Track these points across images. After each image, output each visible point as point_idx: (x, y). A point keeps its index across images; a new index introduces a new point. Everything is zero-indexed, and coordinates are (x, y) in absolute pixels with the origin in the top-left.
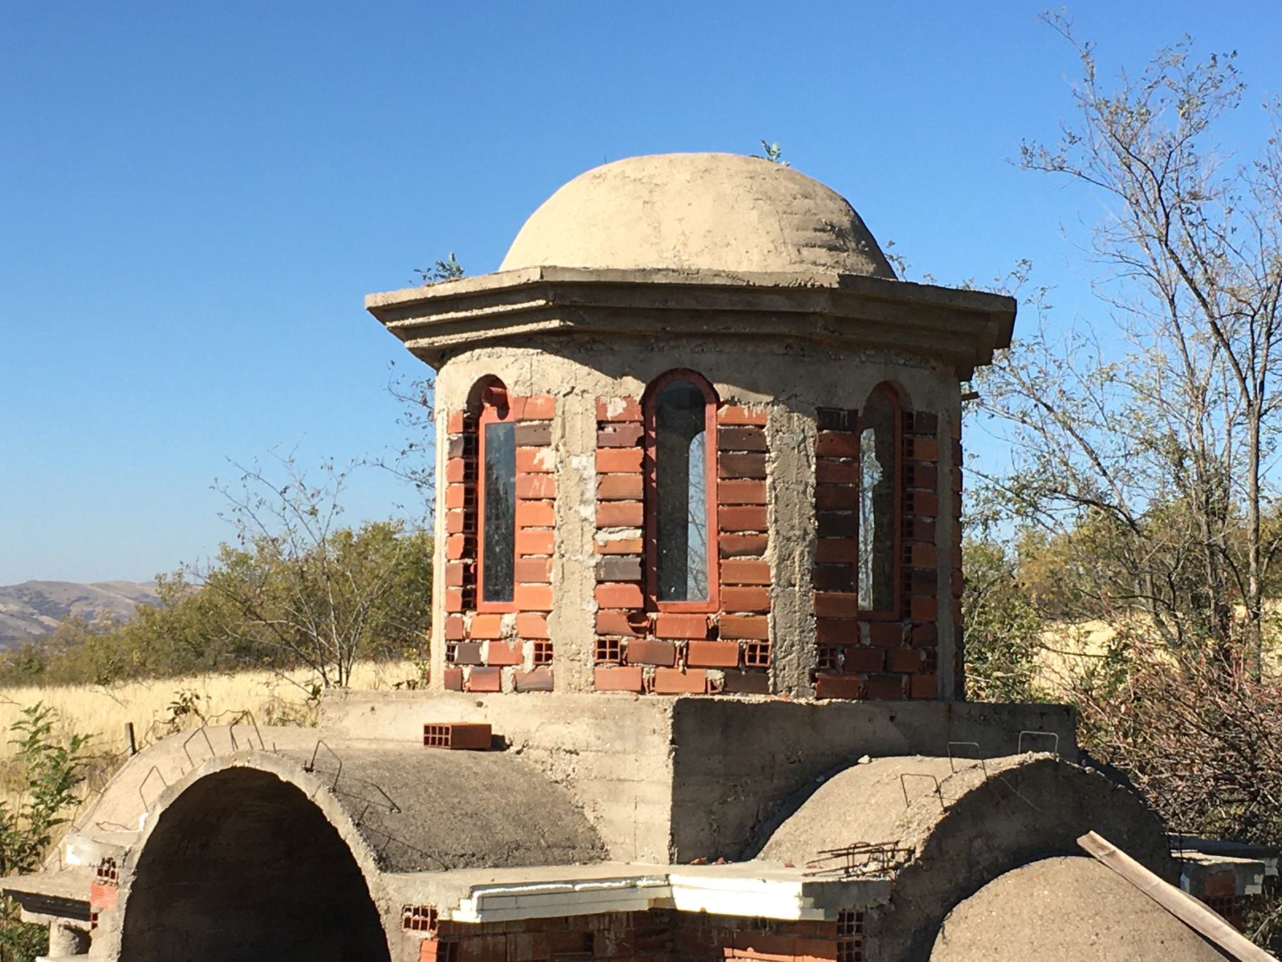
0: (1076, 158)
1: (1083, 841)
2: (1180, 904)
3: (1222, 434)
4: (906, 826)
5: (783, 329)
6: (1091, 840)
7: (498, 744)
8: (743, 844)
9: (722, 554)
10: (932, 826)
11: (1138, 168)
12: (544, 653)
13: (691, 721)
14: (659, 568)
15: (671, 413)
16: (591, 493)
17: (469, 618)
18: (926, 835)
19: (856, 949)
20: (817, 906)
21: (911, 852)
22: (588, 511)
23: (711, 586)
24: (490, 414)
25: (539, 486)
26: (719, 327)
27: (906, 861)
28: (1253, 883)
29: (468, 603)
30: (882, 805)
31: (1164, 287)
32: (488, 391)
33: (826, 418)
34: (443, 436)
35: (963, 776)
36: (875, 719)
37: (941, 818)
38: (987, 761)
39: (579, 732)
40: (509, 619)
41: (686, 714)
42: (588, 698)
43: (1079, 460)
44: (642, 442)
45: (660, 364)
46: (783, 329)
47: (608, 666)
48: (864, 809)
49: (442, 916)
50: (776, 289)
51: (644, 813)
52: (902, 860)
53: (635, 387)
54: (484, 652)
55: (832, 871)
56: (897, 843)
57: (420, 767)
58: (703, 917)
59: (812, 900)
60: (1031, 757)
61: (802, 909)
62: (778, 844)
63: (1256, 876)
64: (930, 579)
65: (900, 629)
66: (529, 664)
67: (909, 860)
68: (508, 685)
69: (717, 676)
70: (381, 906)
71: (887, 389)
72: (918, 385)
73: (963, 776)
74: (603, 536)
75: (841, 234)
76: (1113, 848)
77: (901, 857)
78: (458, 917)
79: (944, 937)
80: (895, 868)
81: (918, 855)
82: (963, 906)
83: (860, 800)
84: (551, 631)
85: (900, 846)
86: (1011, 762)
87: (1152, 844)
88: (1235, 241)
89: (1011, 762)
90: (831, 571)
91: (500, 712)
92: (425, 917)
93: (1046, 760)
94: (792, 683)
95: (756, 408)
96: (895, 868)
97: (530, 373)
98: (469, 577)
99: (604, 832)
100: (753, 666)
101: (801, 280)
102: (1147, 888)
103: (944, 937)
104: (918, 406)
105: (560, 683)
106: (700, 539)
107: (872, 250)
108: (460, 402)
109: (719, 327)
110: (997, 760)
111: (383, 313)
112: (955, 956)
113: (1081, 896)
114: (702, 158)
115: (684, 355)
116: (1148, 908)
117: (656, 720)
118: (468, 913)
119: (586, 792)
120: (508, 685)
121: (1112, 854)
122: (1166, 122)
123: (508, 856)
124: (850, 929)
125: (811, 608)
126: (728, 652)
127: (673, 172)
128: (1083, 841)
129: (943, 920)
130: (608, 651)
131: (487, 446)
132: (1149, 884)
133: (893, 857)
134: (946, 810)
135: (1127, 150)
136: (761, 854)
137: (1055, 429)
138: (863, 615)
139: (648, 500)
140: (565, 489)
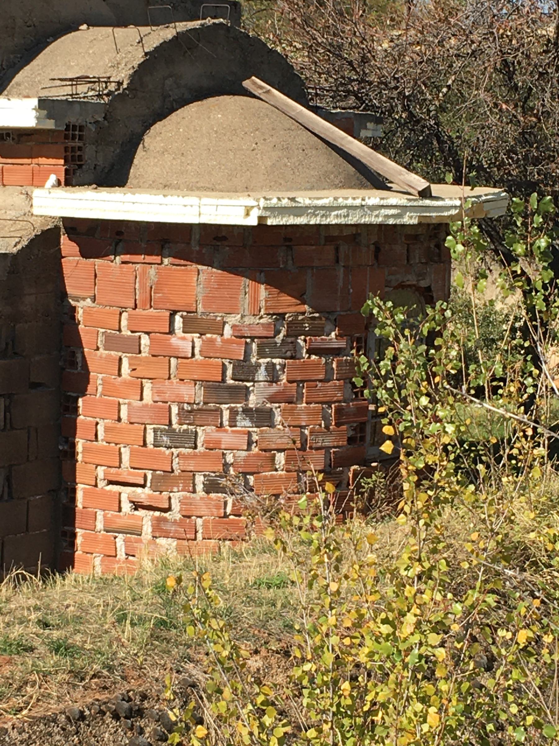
1: (246, 84)
2: (317, 124)
4: (116, 66)
6: (253, 83)
10: (136, 66)
18: (132, 71)
19: (78, 153)
20: (49, 117)
21: (120, 84)
27: (116, 90)
28: (366, 128)
37: (142, 60)
38: (177, 24)
48: (84, 56)
52: (113, 89)
55: (61, 92)
56: (109, 78)
59: (45, 112)
60: (209, 21)
61: (38, 118)
62: (18, 84)
63: (368, 124)
67: (118, 89)
76: (269, 87)
77: (112, 87)
79: (144, 147)
80: (107, 95)
81: (125, 86)
82: (158, 126)
83: (80, 51)
85: (111, 80)
86: (196, 24)
87: (292, 84)
89: (196, 24)
93: (221, 24)
96: (107, 95)
102: (292, 114)
103: (144, 147)
110: (184, 23)
112: (152, 159)
113: (245, 118)
116: (293, 127)
121: (268, 92)
124: (74, 138)
128: (246, 84)
129: (143, 135)
132: (294, 111)
133: (106, 87)
134: (146, 54)
136: (5, 92)
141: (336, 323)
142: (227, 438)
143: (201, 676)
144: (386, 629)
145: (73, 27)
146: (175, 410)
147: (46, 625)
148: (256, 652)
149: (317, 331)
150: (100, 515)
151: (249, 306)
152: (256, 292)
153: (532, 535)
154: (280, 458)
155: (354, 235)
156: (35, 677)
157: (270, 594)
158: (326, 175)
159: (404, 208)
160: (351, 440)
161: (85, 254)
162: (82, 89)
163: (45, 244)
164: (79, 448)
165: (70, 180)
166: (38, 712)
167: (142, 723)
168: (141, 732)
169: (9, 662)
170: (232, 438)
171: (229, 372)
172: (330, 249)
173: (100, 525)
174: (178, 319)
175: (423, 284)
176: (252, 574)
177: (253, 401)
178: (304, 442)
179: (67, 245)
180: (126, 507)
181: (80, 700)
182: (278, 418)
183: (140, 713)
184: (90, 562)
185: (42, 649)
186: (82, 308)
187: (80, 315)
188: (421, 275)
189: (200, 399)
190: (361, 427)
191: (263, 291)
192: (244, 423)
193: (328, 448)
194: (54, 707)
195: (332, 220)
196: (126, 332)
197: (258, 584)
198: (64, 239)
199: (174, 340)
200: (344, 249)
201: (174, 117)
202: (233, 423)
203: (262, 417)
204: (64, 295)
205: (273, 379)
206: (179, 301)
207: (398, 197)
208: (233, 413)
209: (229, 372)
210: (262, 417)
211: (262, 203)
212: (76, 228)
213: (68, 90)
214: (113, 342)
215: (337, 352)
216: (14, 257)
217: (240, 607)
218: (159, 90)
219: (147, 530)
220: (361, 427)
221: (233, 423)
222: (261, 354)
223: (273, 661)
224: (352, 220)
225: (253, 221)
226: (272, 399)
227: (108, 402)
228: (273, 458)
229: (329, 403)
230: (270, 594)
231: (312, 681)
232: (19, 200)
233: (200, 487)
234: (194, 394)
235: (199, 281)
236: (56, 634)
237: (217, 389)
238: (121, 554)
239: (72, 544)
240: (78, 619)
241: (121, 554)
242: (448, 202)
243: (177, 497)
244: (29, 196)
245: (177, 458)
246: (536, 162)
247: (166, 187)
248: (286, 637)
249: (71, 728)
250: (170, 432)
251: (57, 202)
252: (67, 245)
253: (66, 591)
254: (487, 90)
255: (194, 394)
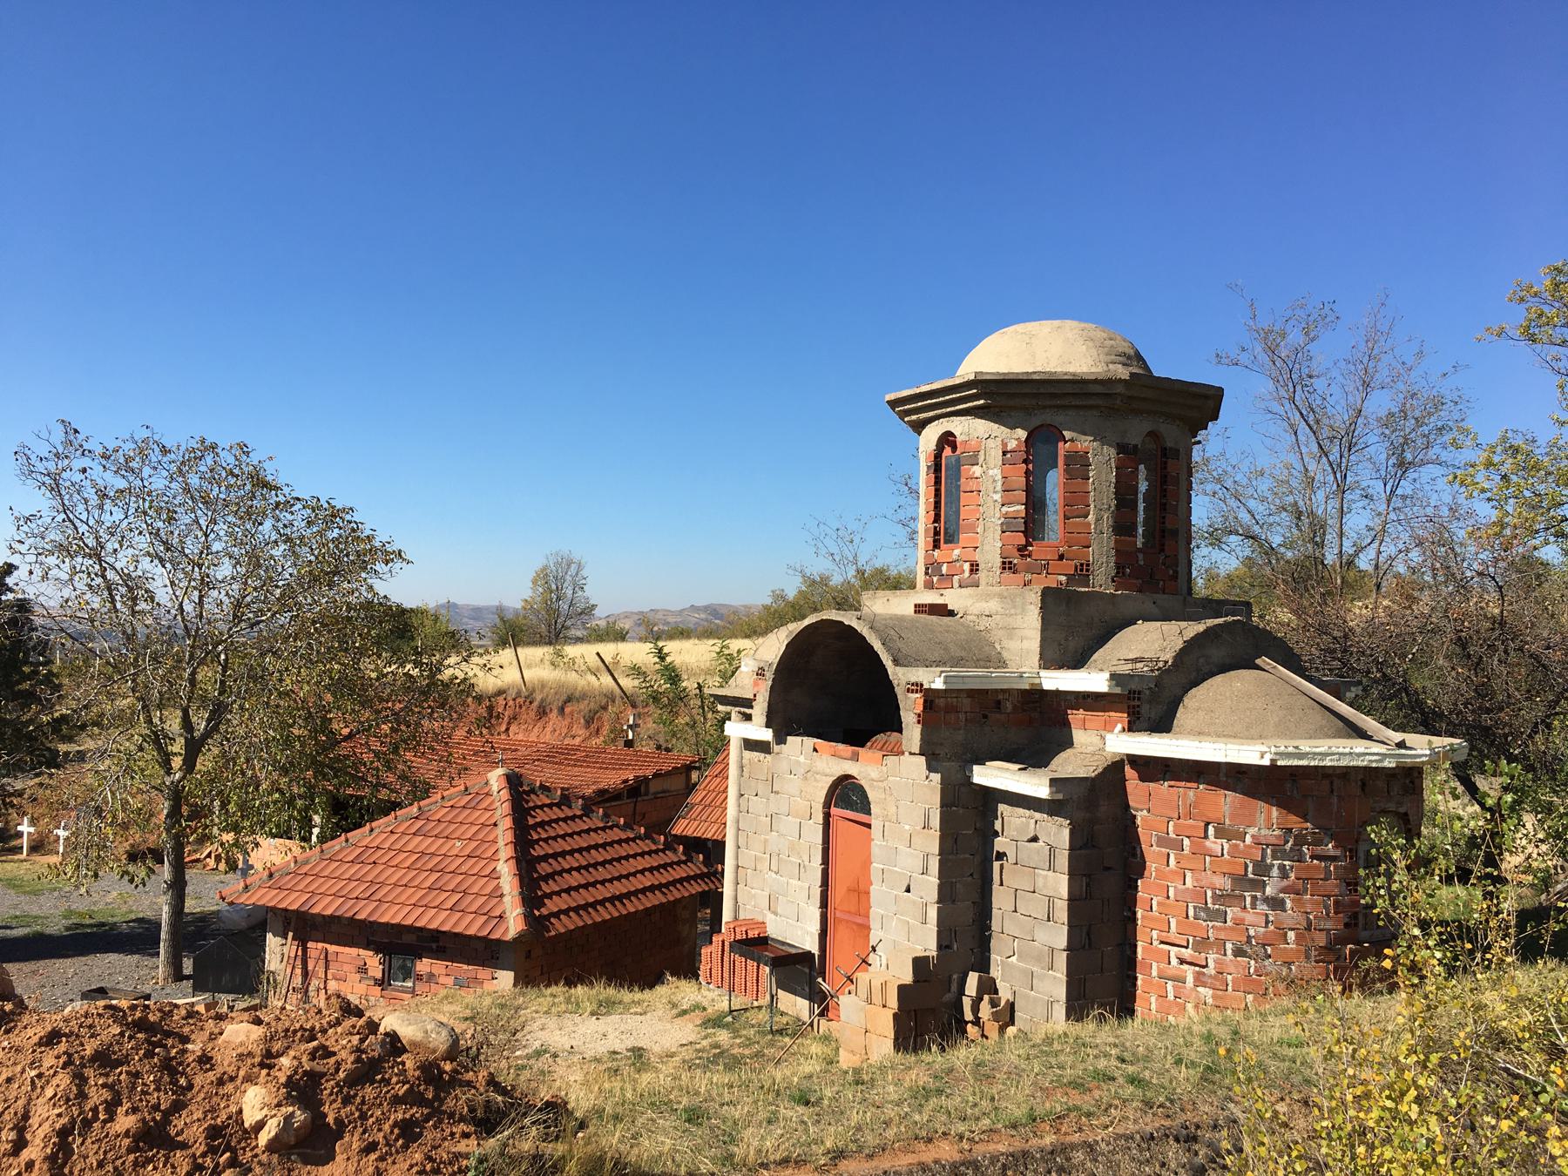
0: (1244, 358)
1: (1258, 661)
3: (1322, 503)
4: (1163, 650)
5: (1100, 402)
6: (1263, 661)
7: (951, 613)
8: (1077, 662)
9: (1066, 518)
11: (1279, 363)
12: (975, 568)
13: (1050, 598)
14: (1032, 524)
15: (1037, 454)
16: (999, 488)
17: (936, 553)
22: (998, 497)
23: (1060, 534)
24: (948, 451)
25: (973, 485)
26: (1066, 402)
29: (936, 545)
30: (1151, 642)
31: (1291, 426)
32: (947, 439)
33: (1121, 448)
34: (924, 463)
35: (1193, 629)
36: (1146, 602)
39: (993, 605)
40: (957, 552)
41: (1046, 593)
42: (997, 589)
43: (1244, 516)
44: (1025, 461)
45: (1036, 422)
46: (1100, 402)
47: (1008, 575)
49: (926, 686)
50: (1096, 381)
51: (1026, 644)
53: (1022, 434)
54: (944, 569)
55: (1125, 669)
57: (912, 620)
58: (1057, 693)
60: (1230, 619)
64: (1175, 533)
65: (1154, 561)
66: (967, 574)
68: (956, 584)
69: (1063, 578)
70: (895, 683)
71: (1153, 435)
72: (1171, 434)
73: (1193, 629)
74: (1005, 509)
75: (1129, 358)
77: (1161, 664)
78: (934, 686)
82: (1194, 691)
84: (978, 557)
87: (1292, 662)
88: (1331, 401)
90: (1123, 527)
91: (952, 598)
92: (917, 687)
94: (1102, 581)
95: (1085, 443)
97: (968, 429)
98: (936, 533)
99: (1005, 655)
100: (1083, 572)
101: (1109, 375)
104: (1169, 445)
105: (983, 582)
106: (1054, 518)
107: (1146, 368)
108: (932, 446)
109: (1066, 402)
111: (893, 404)
114: (1057, 323)
115: (1047, 417)
117: (1033, 598)
118: (939, 684)
119: (996, 635)
120: (956, 584)
122: (1295, 337)
123: (958, 662)
125: (1112, 544)
126: (1069, 566)
127: (1042, 329)
128: (1258, 661)
130: (1007, 566)
131: (947, 465)
135: (1272, 351)
137: (1233, 503)
138: (1139, 550)
139: (1029, 490)
140: (986, 485)
141: (1332, 838)
142: (1249, 917)
143: (1241, 1116)
144: (1389, 1104)
145: (1132, 622)
146: (1209, 893)
147: (1123, 1061)
148: (1282, 1099)
149: (1318, 842)
150: (1155, 965)
151: (1265, 822)
152: (1269, 813)
153: (1504, 1023)
154: (1291, 935)
155: (1345, 773)
156: (1116, 1102)
157: (1291, 1052)
158: (1321, 728)
159: (1384, 756)
160: (1347, 925)
161: (1142, 779)
162: (1139, 665)
163: (1115, 770)
164: (1139, 915)
165: (1131, 728)
166: (1120, 1131)
167: (1196, 1147)
168: (1196, 1154)
169: (1098, 1088)
170: (1254, 918)
171: (1250, 869)
172: (1326, 782)
173: (1154, 973)
174: (1211, 830)
175: (1402, 810)
176: (1276, 1034)
177: (1269, 891)
178: (1309, 923)
179: (1129, 772)
180: (1174, 961)
181: (1151, 1124)
182: (1289, 904)
183: (1195, 1139)
184: (1147, 1002)
185: (1121, 1080)
186: (1140, 817)
187: (1139, 821)
188: (1400, 804)
189: (1228, 887)
190: (1355, 916)
191: (1275, 812)
192: (1262, 907)
193: (1328, 931)
194: (1132, 1127)
195: (1328, 763)
196: (1172, 835)
197: (1281, 1042)
198: (1127, 768)
199: (1207, 843)
200: (1337, 782)
201: (1205, 684)
202: (1254, 906)
203: (1276, 904)
204: (1128, 806)
205: (1284, 874)
206: (1211, 815)
207: (1377, 747)
208: (1254, 898)
209: (1250, 869)
210: (1276, 904)
211: (1273, 750)
212: (1136, 761)
213: (1130, 666)
214: (1162, 842)
215: (1334, 859)
216: (1093, 779)
217: (1269, 1062)
218: (1194, 666)
219: (1190, 979)
220: (1355, 916)
221: (1254, 906)
222: (1274, 857)
223: (1296, 1108)
224: (1344, 763)
225: (1266, 762)
226: (1284, 890)
227: (1159, 886)
228: (1285, 935)
229: (1329, 897)
230: (1291, 1052)
231: (1329, 1134)
232: (1096, 740)
233: (1229, 952)
234: (1224, 883)
235: (1226, 802)
236: (1131, 1069)
237: (1240, 880)
238: (1171, 997)
239: (1135, 985)
240: (1147, 1059)
241: (1171, 997)
242: (1419, 752)
243: (1212, 958)
244: (1103, 738)
245: (1212, 929)
246: (1488, 711)
247: (1200, 734)
248: (1305, 1089)
249: (1144, 1146)
250: (1206, 909)
251: (1124, 743)
252: (1129, 772)
253: (1132, 1029)
254: (1446, 657)
255: (1224, 883)
